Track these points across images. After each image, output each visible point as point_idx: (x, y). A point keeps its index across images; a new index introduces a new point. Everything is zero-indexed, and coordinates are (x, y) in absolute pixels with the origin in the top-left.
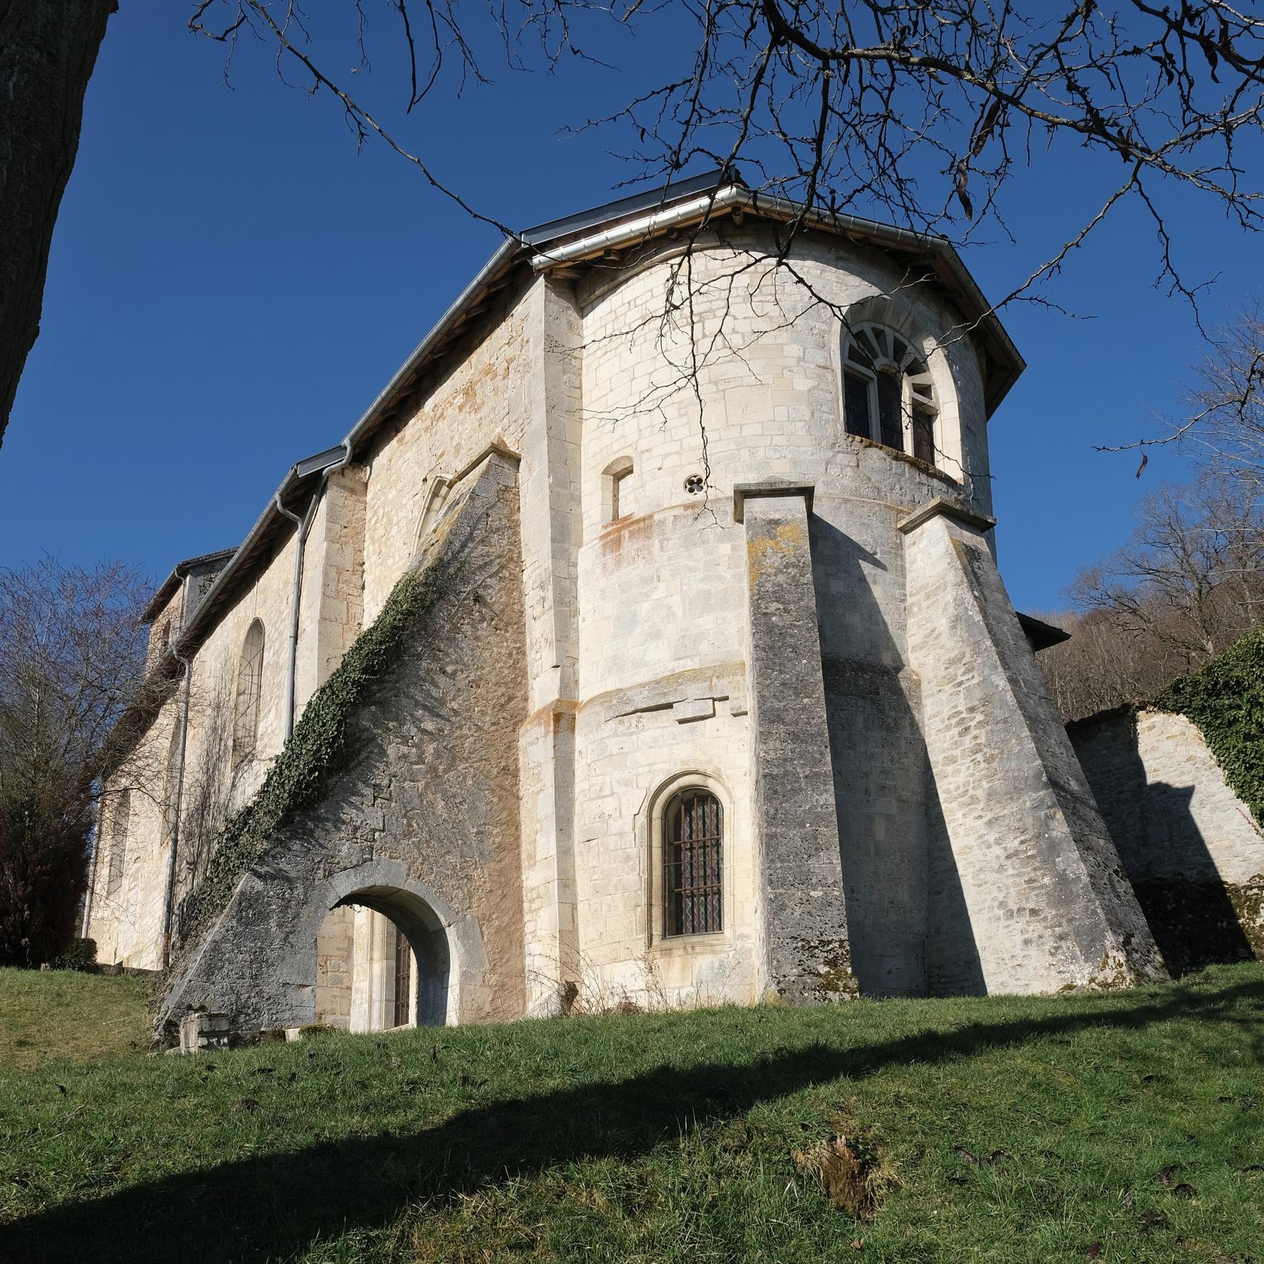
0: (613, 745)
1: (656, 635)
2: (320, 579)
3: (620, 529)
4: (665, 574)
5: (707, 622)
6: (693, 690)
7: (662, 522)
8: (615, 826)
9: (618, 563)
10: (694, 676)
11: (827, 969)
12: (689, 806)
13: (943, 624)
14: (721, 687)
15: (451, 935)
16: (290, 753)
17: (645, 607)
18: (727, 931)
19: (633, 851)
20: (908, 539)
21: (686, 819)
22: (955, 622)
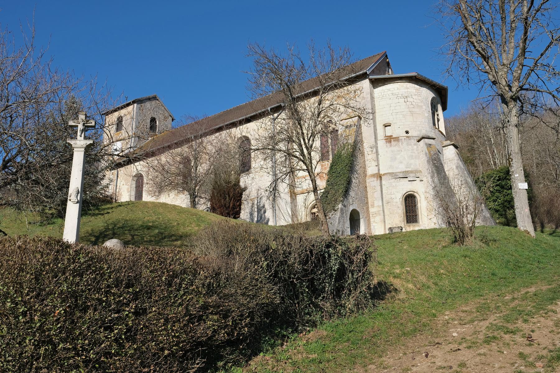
0: (394, 184)
1: (401, 162)
2: (527, 210)
3: (389, 139)
4: (403, 150)
5: (412, 161)
6: (412, 175)
7: (401, 139)
8: (395, 200)
9: (391, 146)
10: (412, 172)
11: (197, 228)
12: (409, 198)
13: (454, 167)
14: (418, 175)
15: (362, 221)
16: (443, 202)
17: (398, 157)
18: (421, 223)
19: (400, 206)
20: (444, 148)
21: (410, 201)
22: (457, 167)
